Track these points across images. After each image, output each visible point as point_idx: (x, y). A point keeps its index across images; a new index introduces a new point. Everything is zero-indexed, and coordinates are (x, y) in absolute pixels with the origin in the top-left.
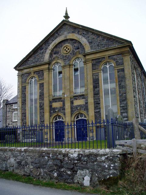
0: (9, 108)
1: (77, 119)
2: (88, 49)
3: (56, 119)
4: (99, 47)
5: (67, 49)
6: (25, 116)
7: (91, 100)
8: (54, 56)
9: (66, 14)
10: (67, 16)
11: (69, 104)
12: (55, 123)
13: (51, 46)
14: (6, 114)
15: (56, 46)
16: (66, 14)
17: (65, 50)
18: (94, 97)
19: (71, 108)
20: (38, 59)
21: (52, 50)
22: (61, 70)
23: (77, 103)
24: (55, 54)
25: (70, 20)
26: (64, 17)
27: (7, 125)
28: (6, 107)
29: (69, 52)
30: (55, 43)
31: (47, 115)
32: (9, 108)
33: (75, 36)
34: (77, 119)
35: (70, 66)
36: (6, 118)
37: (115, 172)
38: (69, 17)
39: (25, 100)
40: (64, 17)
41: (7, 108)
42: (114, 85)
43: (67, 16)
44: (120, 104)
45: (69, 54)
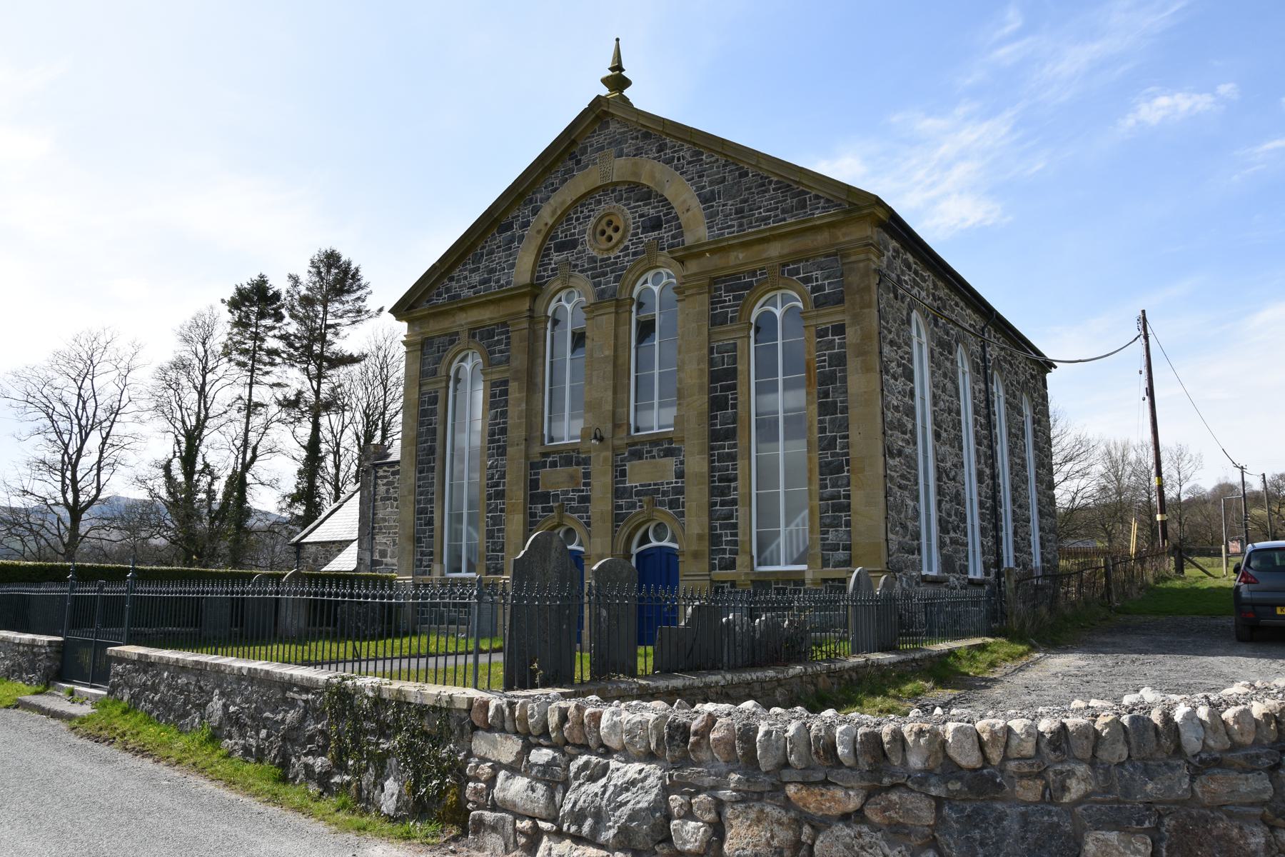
0: (385, 481)
1: (640, 544)
2: (698, 231)
3: (645, 539)
4: (745, 220)
5: (609, 231)
6: (430, 522)
7: (697, 463)
8: (556, 257)
9: (618, 67)
10: (618, 81)
11: (608, 479)
12: (638, 555)
13: (547, 215)
14: (374, 507)
15: (565, 216)
16: (618, 67)
17: (616, 229)
18: (712, 448)
19: (618, 493)
20: (492, 271)
21: (550, 234)
22: (582, 325)
23: (639, 474)
24: (561, 247)
25: (641, 97)
26: (605, 81)
27: (377, 557)
28: (376, 478)
29: (620, 242)
30: (563, 202)
31: (515, 522)
32: (385, 481)
33: (652, 171)
34: (640, 544)
35: (617, 307)
36: (373, 528)
37: (351, 739)
38: (626, 83)
39: (432, 451)
40: (605, 81)
41: (379, 482)
42: (799, 398)
43: (618, 81)
44: (824, 487)
45: (617, 252)
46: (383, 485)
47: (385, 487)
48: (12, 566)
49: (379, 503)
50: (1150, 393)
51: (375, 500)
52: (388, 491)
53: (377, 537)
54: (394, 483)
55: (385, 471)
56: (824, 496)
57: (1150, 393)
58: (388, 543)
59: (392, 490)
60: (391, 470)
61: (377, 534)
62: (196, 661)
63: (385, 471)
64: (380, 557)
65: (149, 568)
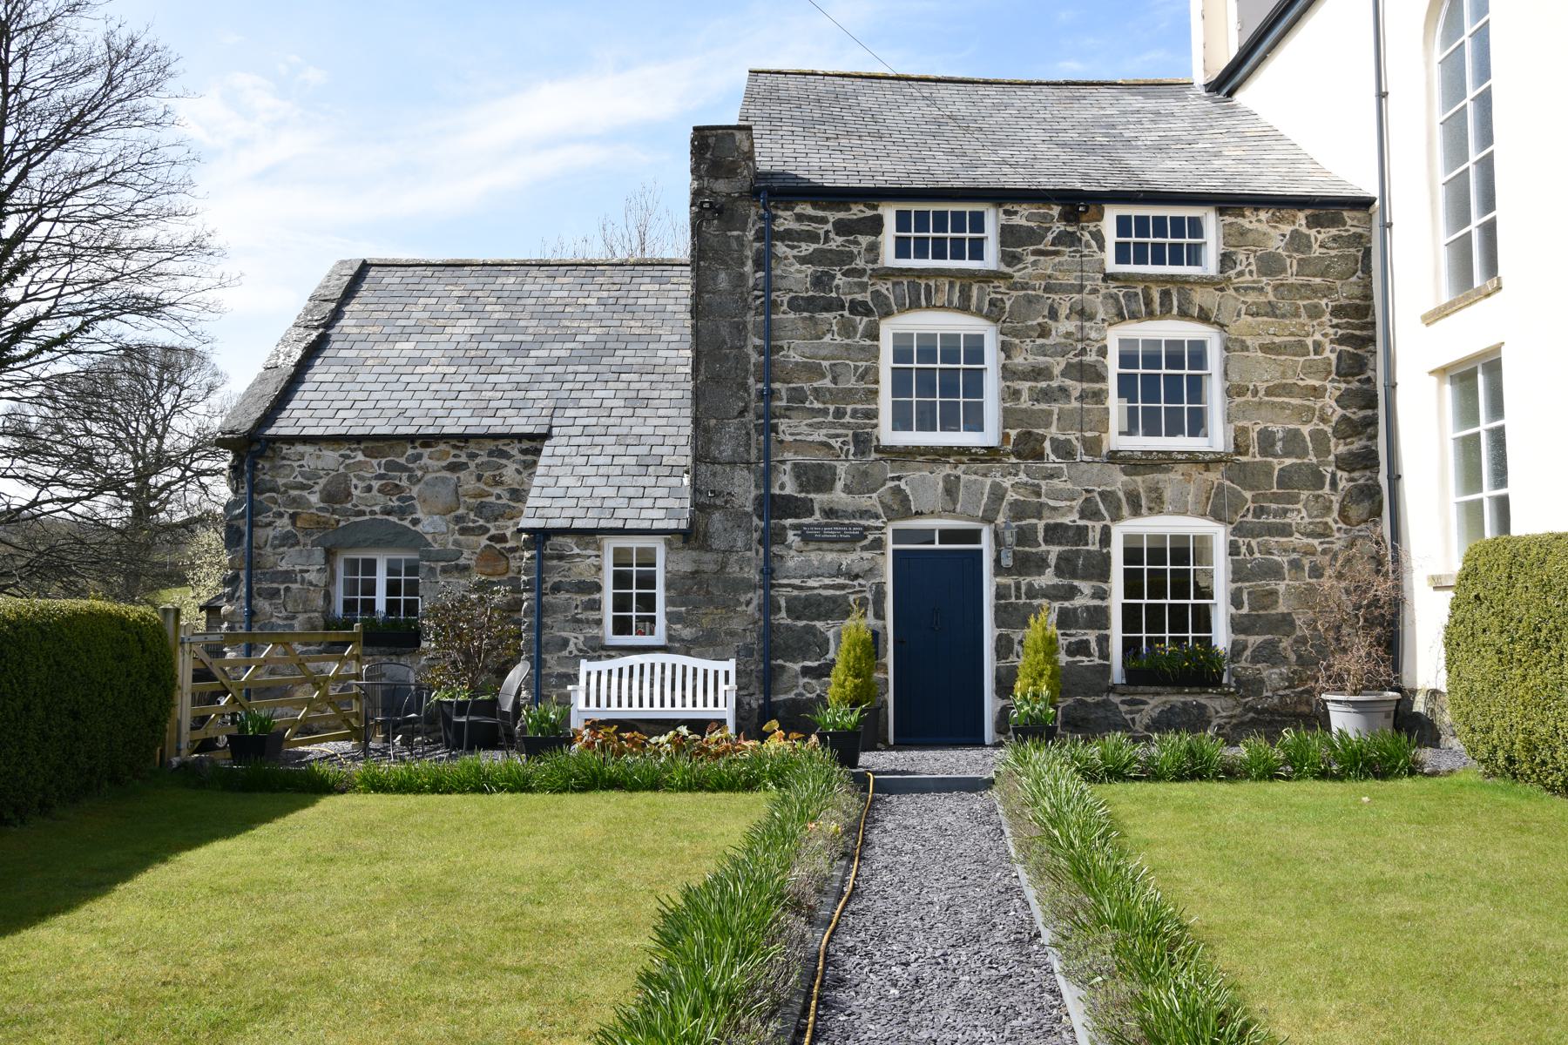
0: (807, 248)
27: (786, 484)
28: (767, 236)
32: (807, 248)
41: (781, 248)
46: (803, 260)
47: (809, 269)
48: (92, 614)
49: (785, 316)
50: (1382, 95)
51: (771, 306)
52: (820, 281)
53: (783, 424)
54: (851, 257)
55: (800, 218)
56: (1256, 293)
57: (1382, 95)
58: (836, 443)
59: (840, 280)
60: (832, 216)
61: (786, 413)
62: (1451, 643)
63: (800, 218)
64: (802, 488)
65: (1310, 445)
